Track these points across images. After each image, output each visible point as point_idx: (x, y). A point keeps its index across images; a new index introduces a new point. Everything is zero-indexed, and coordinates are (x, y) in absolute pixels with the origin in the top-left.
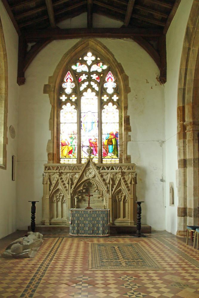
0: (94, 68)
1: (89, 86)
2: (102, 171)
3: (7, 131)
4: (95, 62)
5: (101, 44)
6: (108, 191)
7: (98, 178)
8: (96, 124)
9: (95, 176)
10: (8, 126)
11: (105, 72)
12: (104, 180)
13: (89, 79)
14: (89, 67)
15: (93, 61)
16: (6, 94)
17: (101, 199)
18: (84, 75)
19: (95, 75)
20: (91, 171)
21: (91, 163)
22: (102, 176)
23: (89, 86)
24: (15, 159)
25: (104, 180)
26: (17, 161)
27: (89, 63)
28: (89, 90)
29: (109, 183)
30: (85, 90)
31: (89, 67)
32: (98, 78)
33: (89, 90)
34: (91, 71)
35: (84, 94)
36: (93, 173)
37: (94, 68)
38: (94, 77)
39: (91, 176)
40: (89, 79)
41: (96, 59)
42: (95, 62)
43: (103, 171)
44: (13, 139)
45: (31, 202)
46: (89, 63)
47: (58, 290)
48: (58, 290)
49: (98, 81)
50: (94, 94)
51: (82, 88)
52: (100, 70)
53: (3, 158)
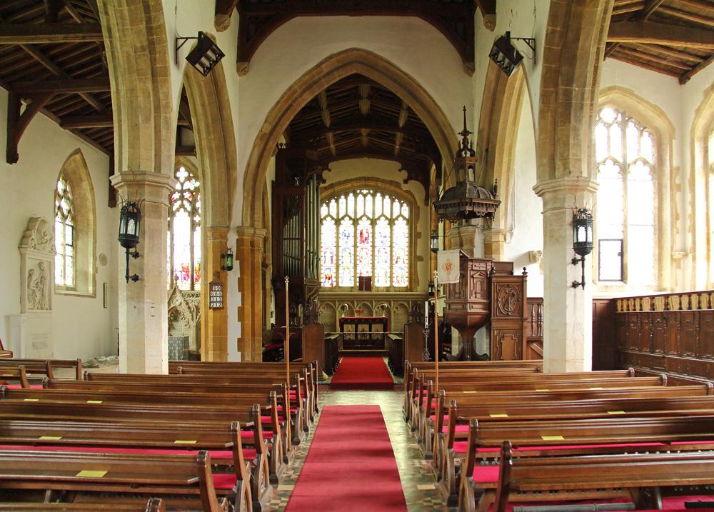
0: (188, 185)
1: (182, 206)
2: (187, 299)
3: (96, 260)
4: (189, 179)
5: (189, 160)
6: (193, 319)
7: (184, 305)
8: (189, 247)
9: (181, 304)
10: (98, 255)
11: (197, 190)
12: (189, 308)
13: (182, 198)
14: (182, 185)
15: (186, 178)
16: (95, 225)
17: (188, 326)
18: (177, 193)
19: (187, 193)
20: (177, 298)
21: (177, 290)
22: (187, 304)
23: (182, 206)
24: (108, 286)
25: (189, 308)
26: (111, 288)
27: (182, 180)
28: (182, 210)
29: (193, 311)
30: (178, 210)
31: (182, 185)
32: (190, 197)
33: (182, 210)
34: (184, 188)
35: (177, 214)
36: (179, 301)
37: (188, 185)
38: (187, 195)
39: (177, 303)
40: (182, 198)
41: (189, 176)
42: (189, 179)
43: (189, 298)
44: (105, 267)
45: (370, 275)
46: (182, 180)
47: (411, 476)
48: (411, 476)
49: (191, 200)
50: (187, 214)
51: (175, 208)
52: (192, 188)
53: (93, 286)
